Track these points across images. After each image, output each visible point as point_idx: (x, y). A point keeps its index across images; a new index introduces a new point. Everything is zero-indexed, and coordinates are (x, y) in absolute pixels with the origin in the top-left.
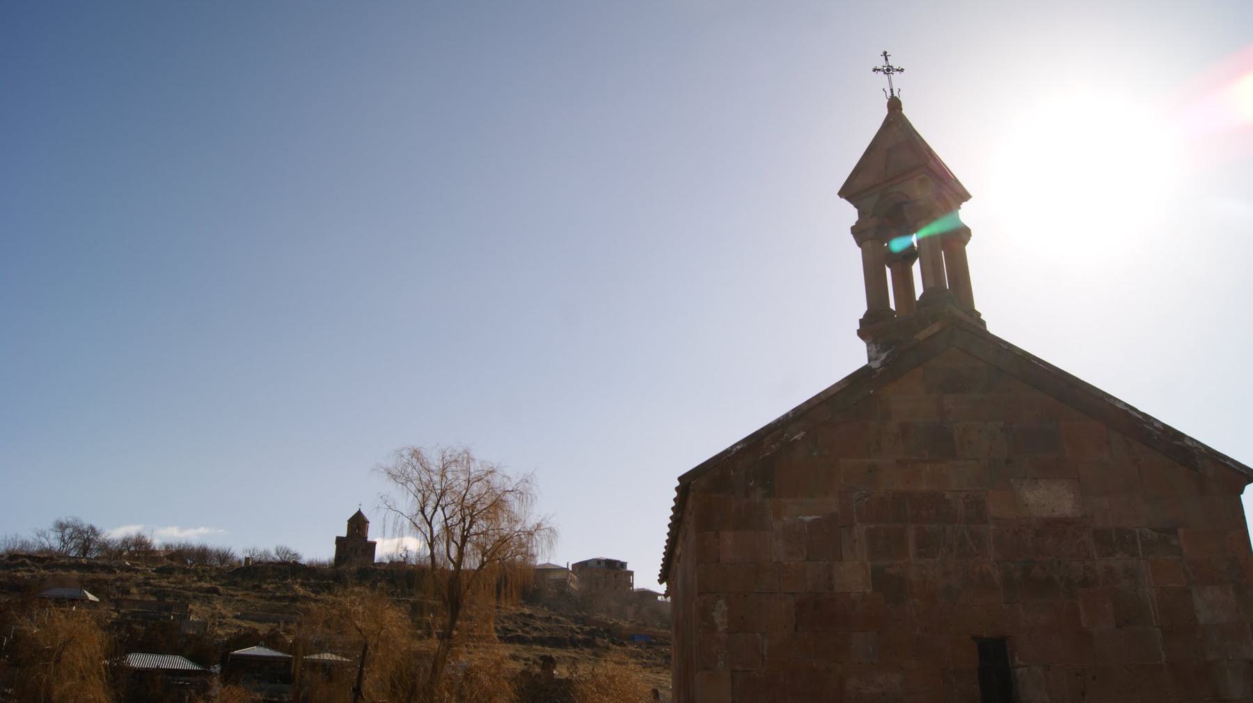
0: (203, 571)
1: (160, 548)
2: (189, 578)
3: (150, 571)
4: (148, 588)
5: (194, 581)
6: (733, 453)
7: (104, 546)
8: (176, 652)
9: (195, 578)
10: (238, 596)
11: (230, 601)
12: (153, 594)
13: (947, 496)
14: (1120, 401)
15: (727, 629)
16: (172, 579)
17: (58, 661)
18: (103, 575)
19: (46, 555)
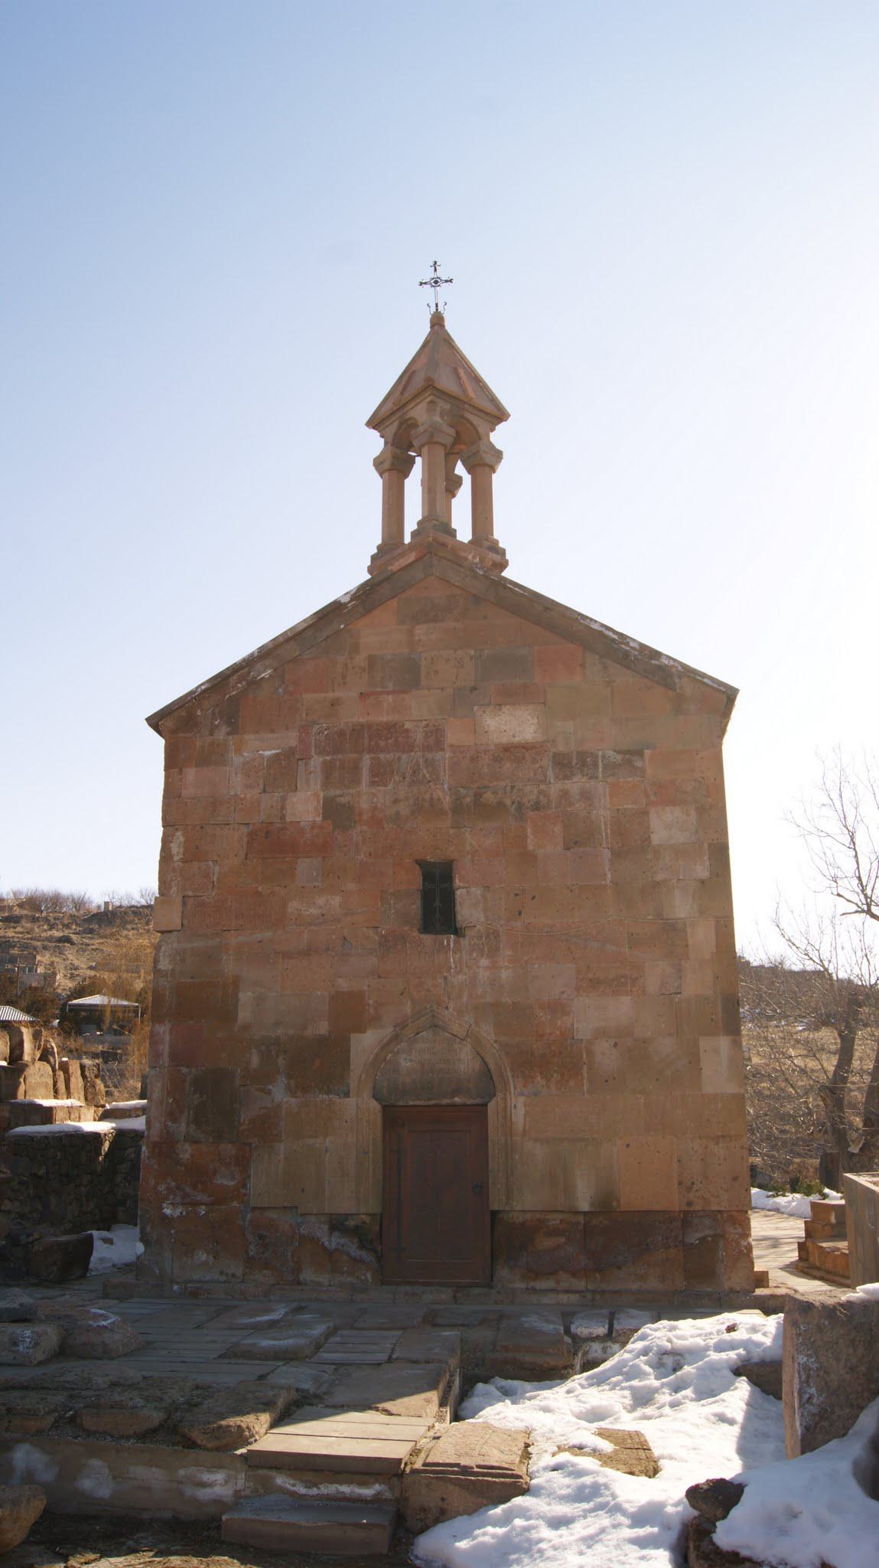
0: (55, 919)
1: (8, 894)
2: (38, 927)
5: (45, 931)
6: (197, 694)
9: (45, 927)
10: (93, 945)
11: (84, 951)
13: (408, 725)
15: (182, 859)
16: (19, 929)
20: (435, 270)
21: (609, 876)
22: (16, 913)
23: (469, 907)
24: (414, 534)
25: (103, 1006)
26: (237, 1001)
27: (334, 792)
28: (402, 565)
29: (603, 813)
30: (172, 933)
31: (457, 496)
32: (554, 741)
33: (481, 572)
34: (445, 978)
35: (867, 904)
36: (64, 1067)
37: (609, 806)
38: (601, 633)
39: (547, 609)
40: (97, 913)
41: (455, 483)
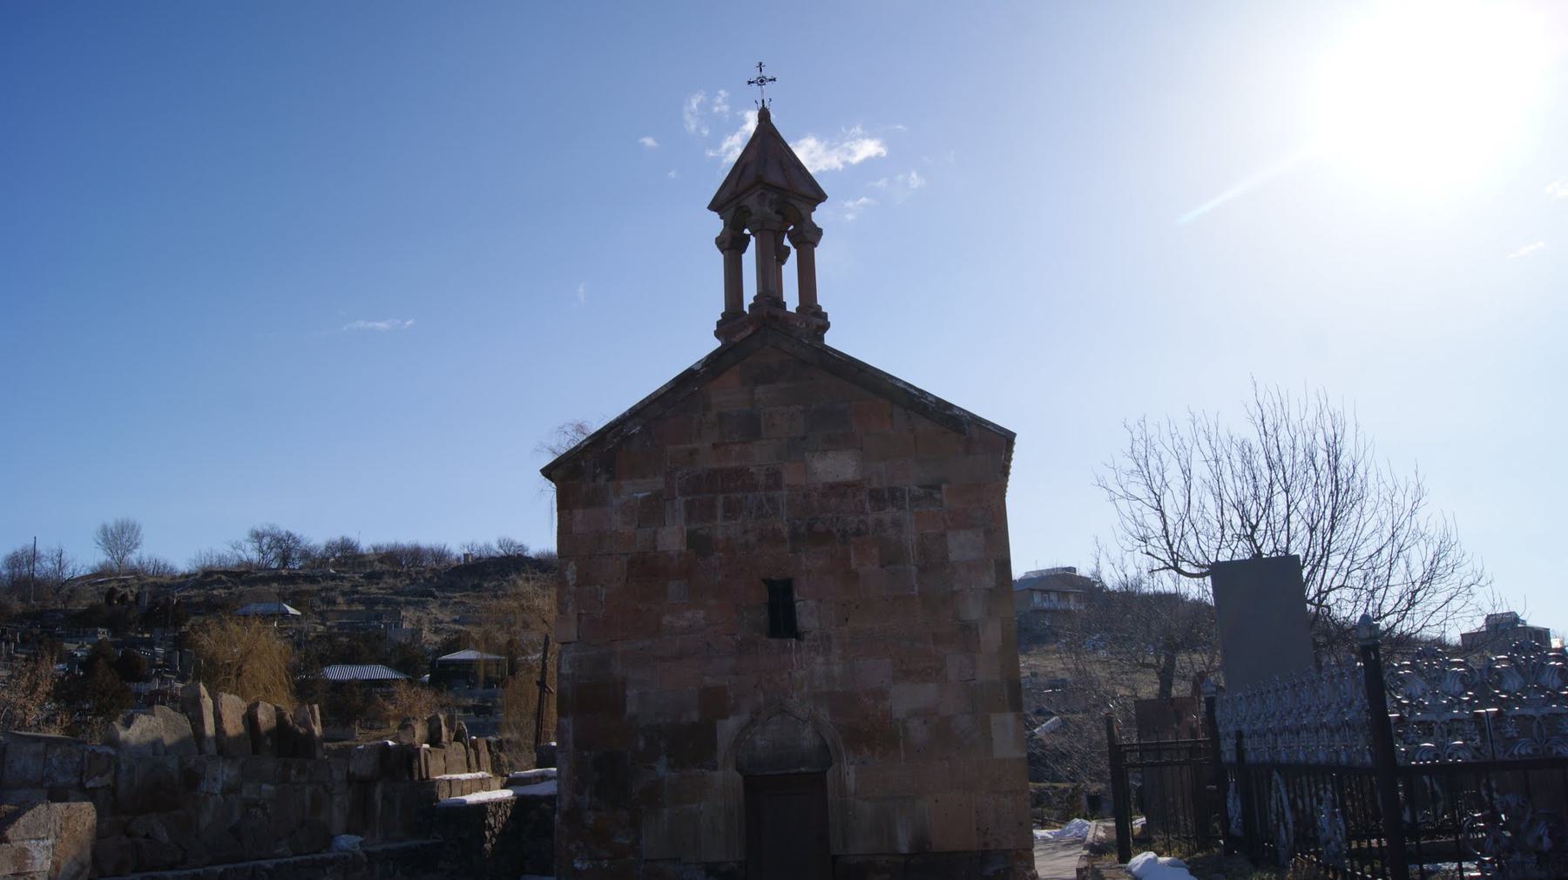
0: (416, 573)
3: (357, 578)
4: (356, 596)
7: (306, 555)
8: (383, 661)
10: (455, 597)
12: (360, 602)
13: (752, 470)
14: (901, 380)
17: (239, 675)
18: (305, 587)
19: (242, 569)
20: (761, 71)
21: (916, 588)
22: (378, 568)
23: (807, 615)
28: (744, 337)
32: (870, 479)
33: (807, 342)
34: (790, 673)
36: (474, 745)
38: (905, 389)
40: (458, 566)
41: (783, 255)
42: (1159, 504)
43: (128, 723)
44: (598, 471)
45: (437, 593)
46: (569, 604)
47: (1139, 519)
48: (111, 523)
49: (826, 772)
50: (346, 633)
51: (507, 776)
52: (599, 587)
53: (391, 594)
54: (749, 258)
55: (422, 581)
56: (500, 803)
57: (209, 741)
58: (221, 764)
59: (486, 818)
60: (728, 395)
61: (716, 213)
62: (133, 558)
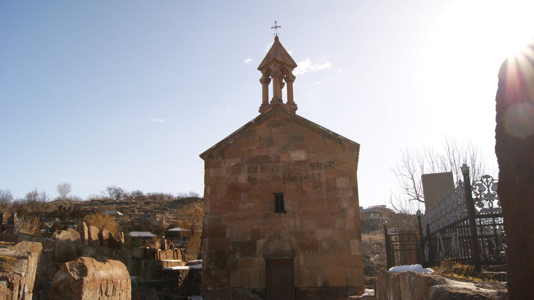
0: (162, 202)
1: (146, 194)
3: (142, 203)
4: (141, 209)
7: (125, 196)
8: (150, 231)
11: (171, 213)
12: (143, 211)
13: (270, 156)
18: (124, 206)
19: (104, 200)
20: (276, 24)
22: (149, 201)
24: (271, 102)
25: (181, 231)
26: (226, 232)
27: (250, 175)
29: (323, 179)
30: (208, 214)
31: (284, 88)
35: (417, 196)
36: (176, 251)
37: (325, 177)
39: (307, 123)
40: (176, 200)
41: (282, 85)
42: (412, 177)
43: (59, 233)
44: (218, 156)
45: (168, 209)
46: (208, 200)
47: (405, 182)
48: (61, 184)
49: (293, 259)
50: (138, 222)
51: (187, 262)
52: (218, 195)
53: (153, 209)
54: (271, 86)
55: (164, 205)
56: (184, 270)
57: (86, 241)
58: (90, 249)
59: (179, 275)
60: (262, 131)
61: (260, 71)
62: (68, 196)
